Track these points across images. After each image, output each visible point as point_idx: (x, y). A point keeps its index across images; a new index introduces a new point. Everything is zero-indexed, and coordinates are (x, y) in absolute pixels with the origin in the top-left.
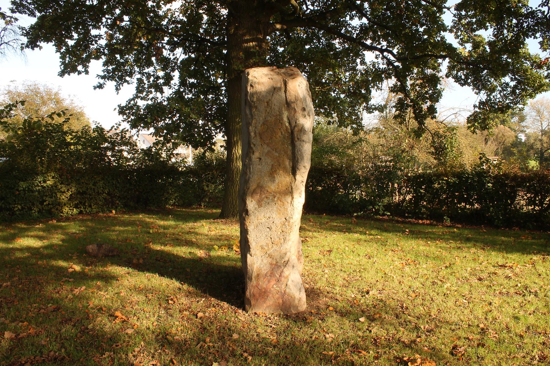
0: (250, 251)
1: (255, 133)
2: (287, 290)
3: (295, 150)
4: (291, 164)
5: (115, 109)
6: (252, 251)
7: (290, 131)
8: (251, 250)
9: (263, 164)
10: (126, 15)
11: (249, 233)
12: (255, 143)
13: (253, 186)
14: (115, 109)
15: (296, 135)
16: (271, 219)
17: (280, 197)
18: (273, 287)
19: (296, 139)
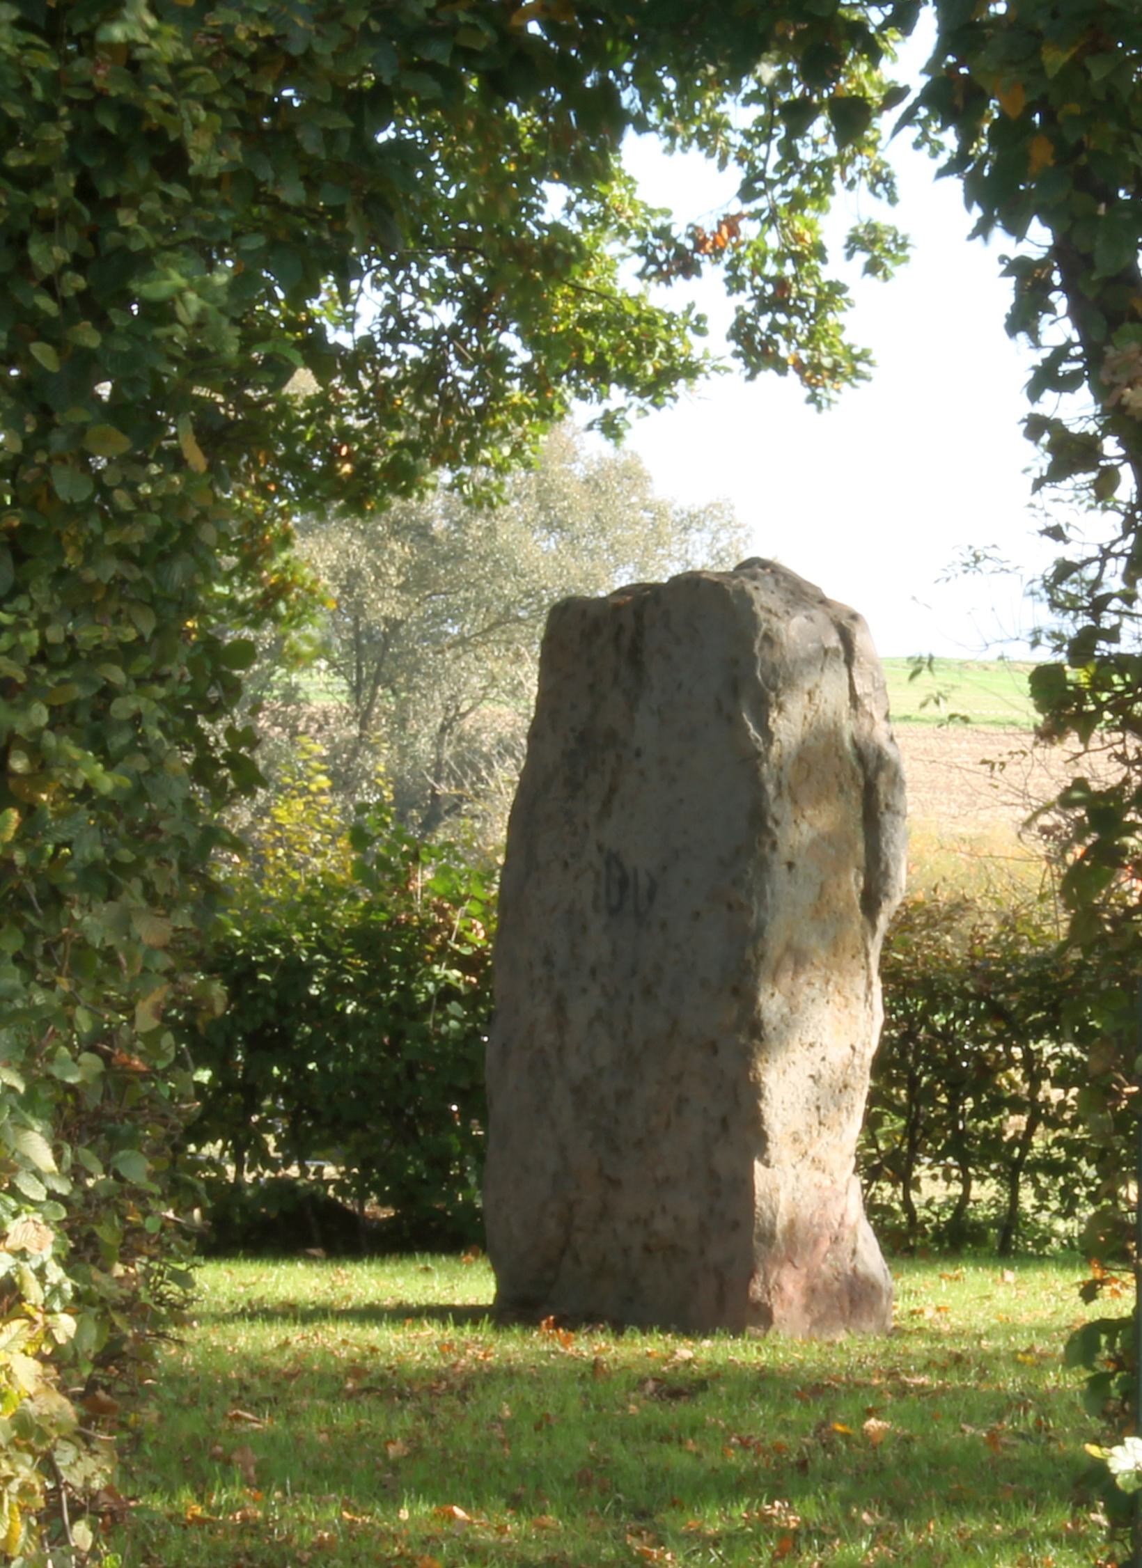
0: (765, 1149)
1: (779, 785)
2: (860, 1268)
3: (878, 841)
4: (861, 883)
5: (1027, 470)
6: (774, 1150)
7: (861, 782)
8: (770, 1145)
9: (800, 881)
10: (1045, 222)
11: (767, 1094)
12: (778, 816)
13: (774, 945)
14: (1027, 470)
15: (882, 797)
16: (817, 1049)
17: (841, 981)
18: (825, 1260)
19: (883, 808)
